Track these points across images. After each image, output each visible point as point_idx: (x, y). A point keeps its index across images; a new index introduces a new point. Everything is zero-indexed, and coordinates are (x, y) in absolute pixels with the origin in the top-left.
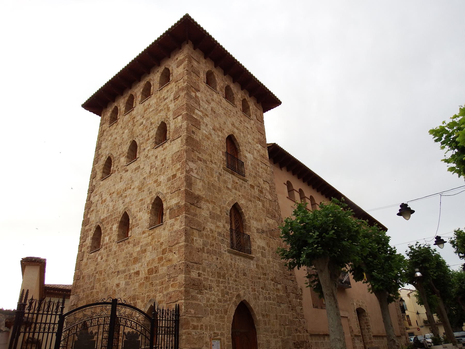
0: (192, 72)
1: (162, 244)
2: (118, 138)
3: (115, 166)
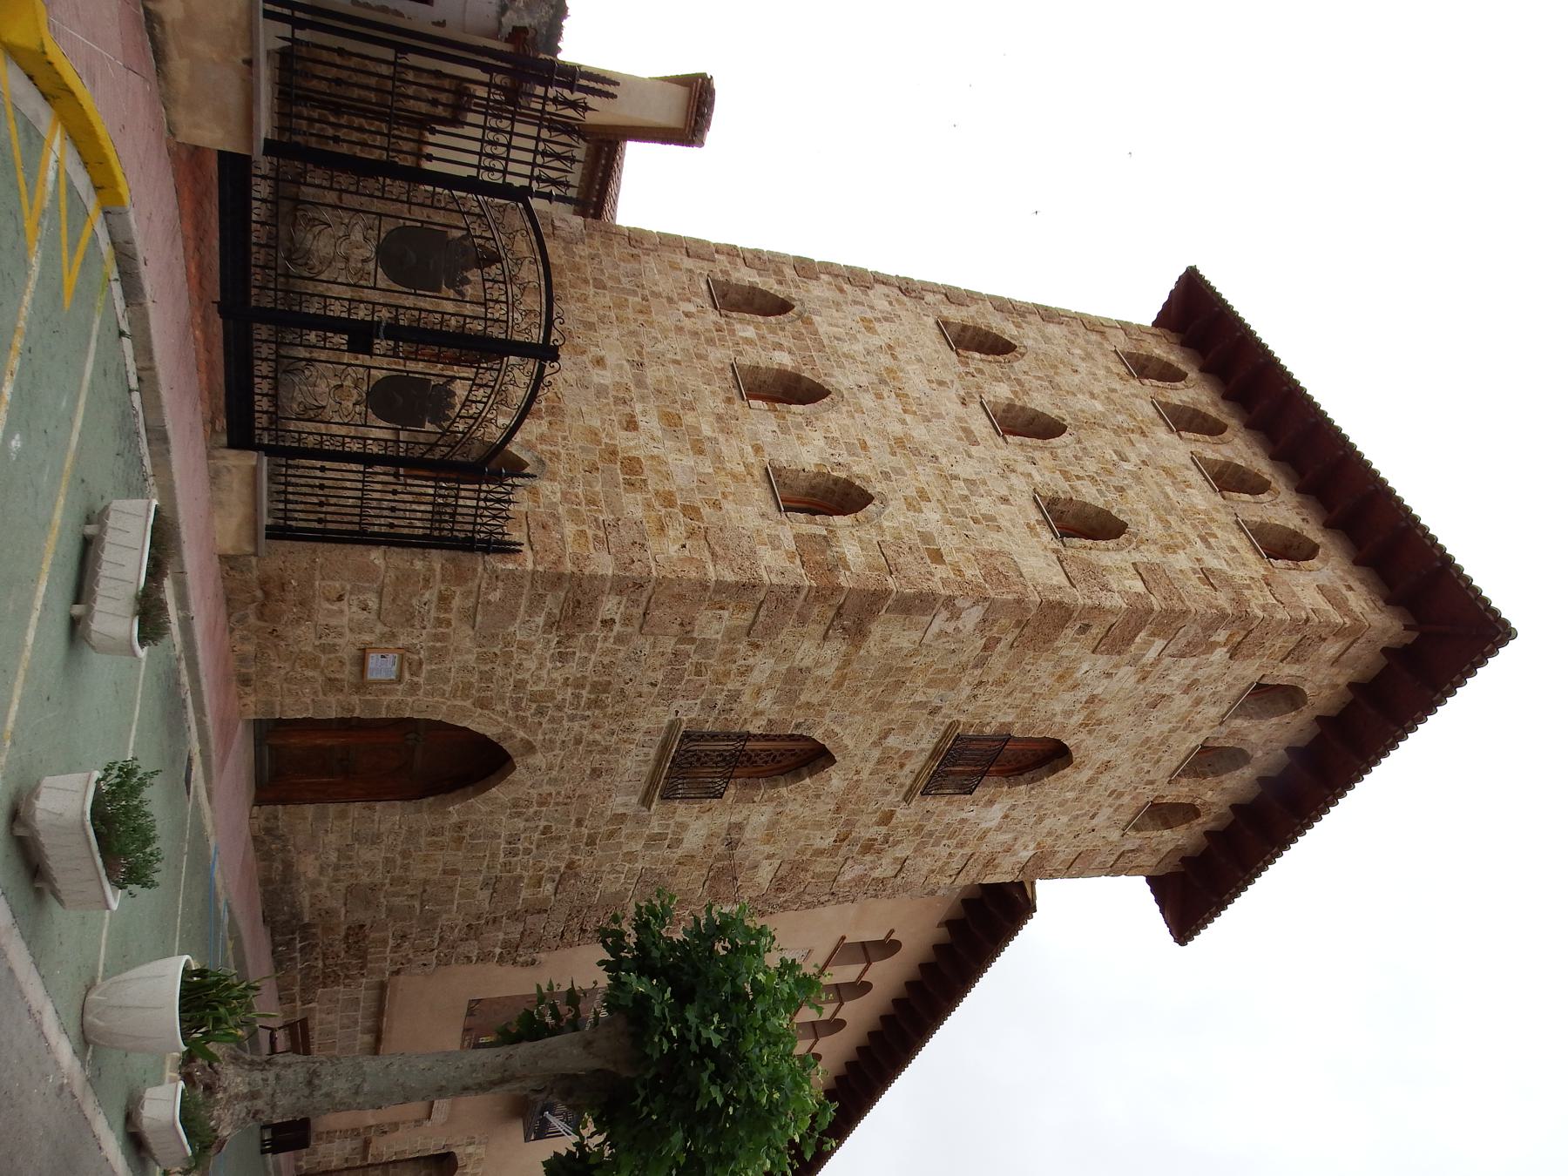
0: (1299, 636)
1: (717, 505)
2: (1076, 379)
3: (981, 365)
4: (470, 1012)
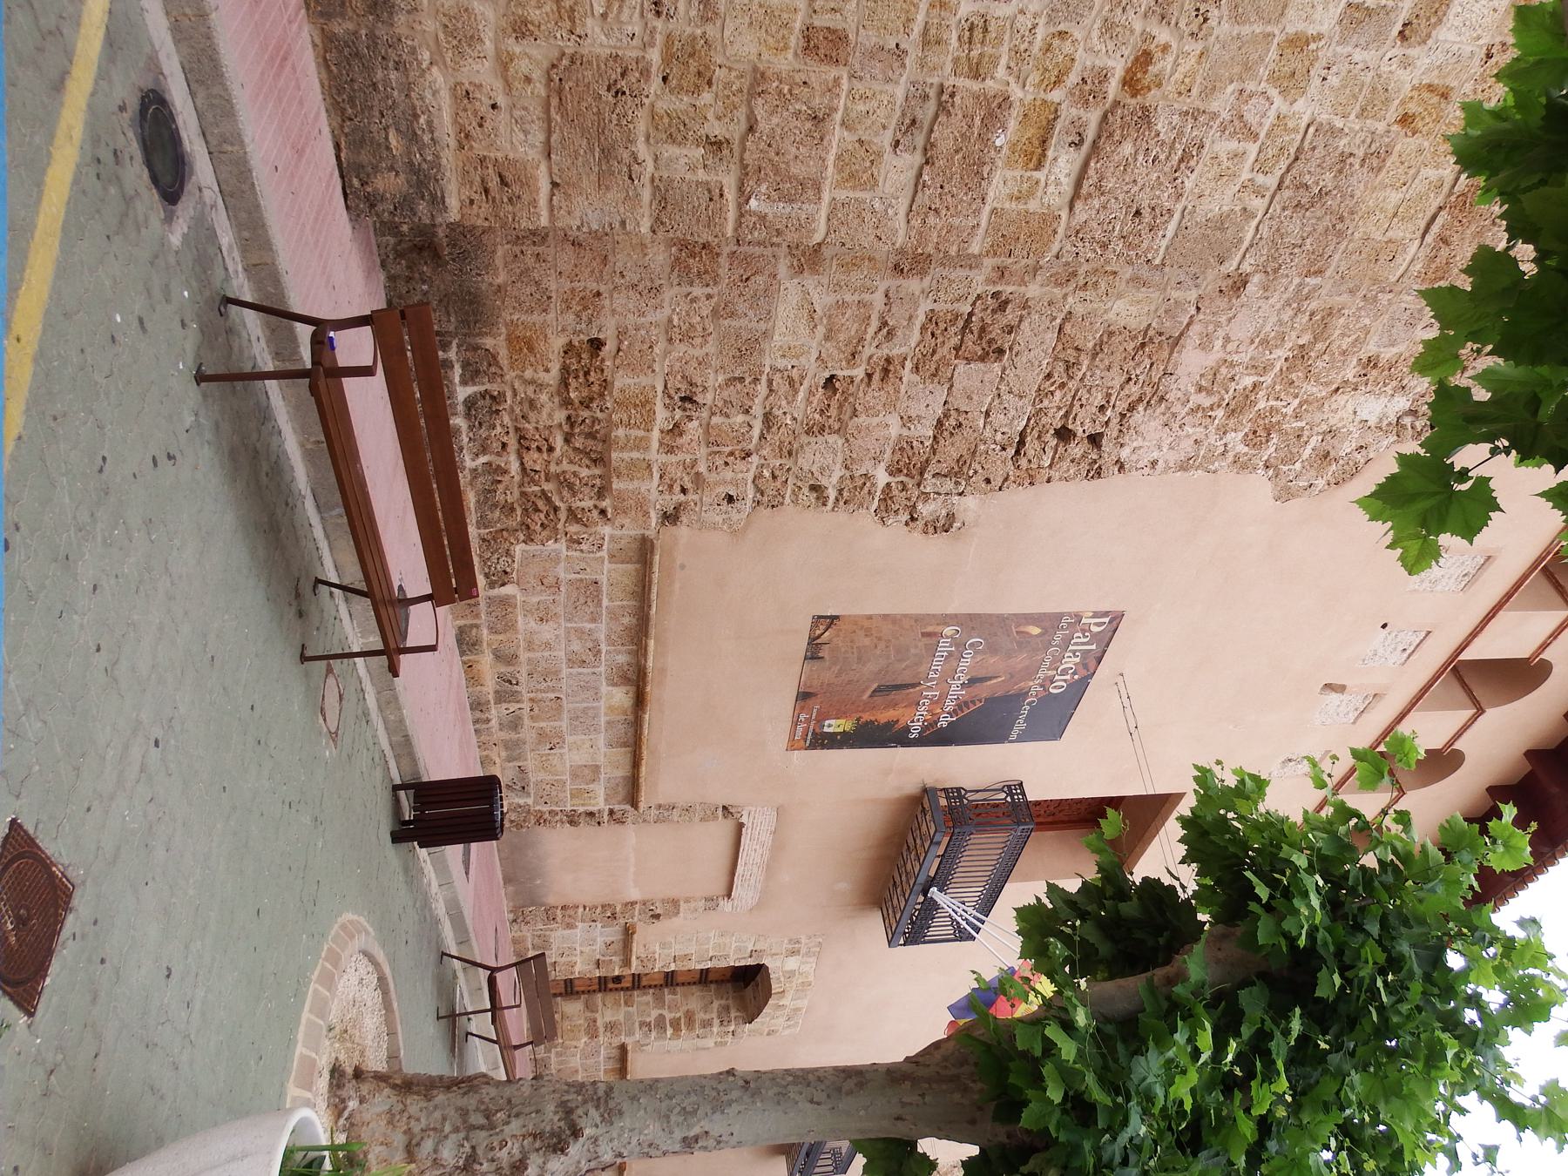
4: (814, 651)
